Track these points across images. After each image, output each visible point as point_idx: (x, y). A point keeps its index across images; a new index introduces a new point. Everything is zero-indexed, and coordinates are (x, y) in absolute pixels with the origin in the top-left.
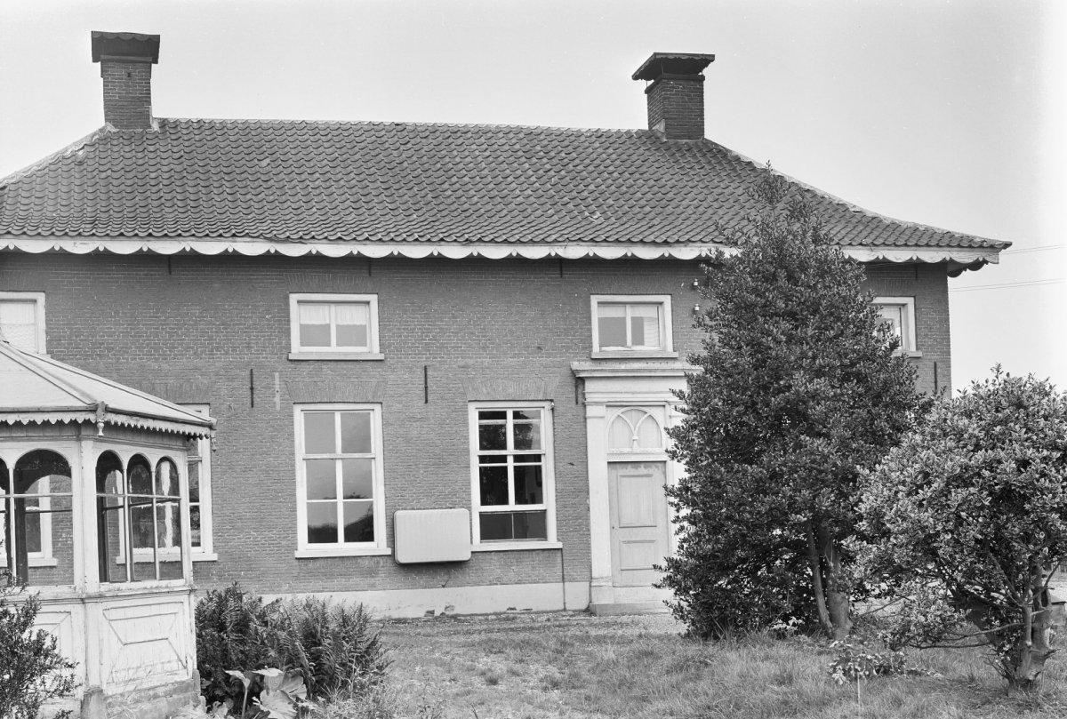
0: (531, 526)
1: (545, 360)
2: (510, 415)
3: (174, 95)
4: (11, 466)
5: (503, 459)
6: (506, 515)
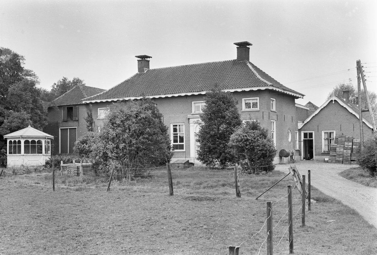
0: (181, 147)
1: (183, 115)
2: (178, 125)
3: (154, 65)
4: (36, 141)
5: (177, 134)
6: (177, 145)
